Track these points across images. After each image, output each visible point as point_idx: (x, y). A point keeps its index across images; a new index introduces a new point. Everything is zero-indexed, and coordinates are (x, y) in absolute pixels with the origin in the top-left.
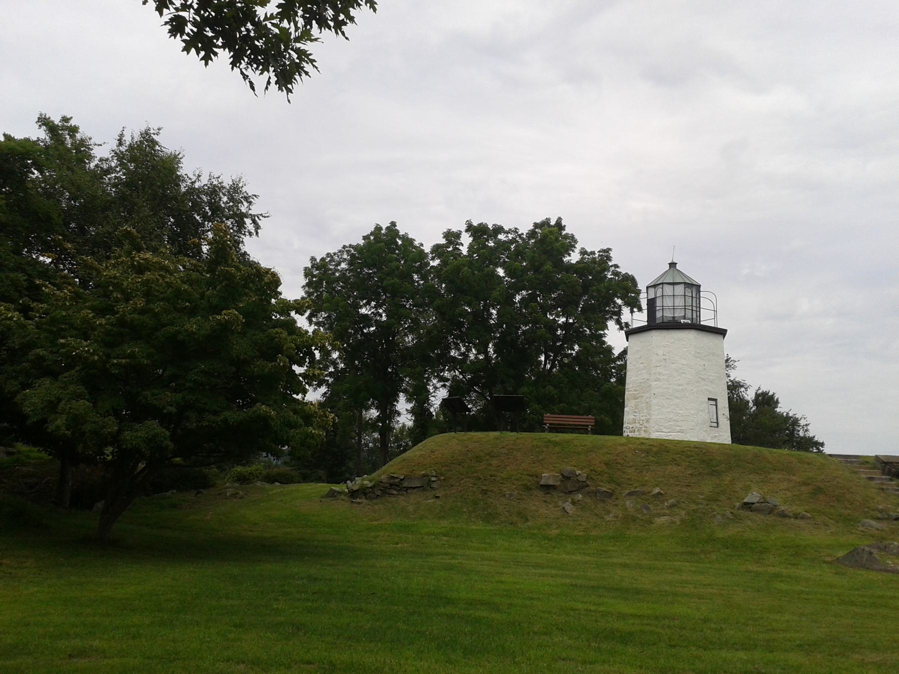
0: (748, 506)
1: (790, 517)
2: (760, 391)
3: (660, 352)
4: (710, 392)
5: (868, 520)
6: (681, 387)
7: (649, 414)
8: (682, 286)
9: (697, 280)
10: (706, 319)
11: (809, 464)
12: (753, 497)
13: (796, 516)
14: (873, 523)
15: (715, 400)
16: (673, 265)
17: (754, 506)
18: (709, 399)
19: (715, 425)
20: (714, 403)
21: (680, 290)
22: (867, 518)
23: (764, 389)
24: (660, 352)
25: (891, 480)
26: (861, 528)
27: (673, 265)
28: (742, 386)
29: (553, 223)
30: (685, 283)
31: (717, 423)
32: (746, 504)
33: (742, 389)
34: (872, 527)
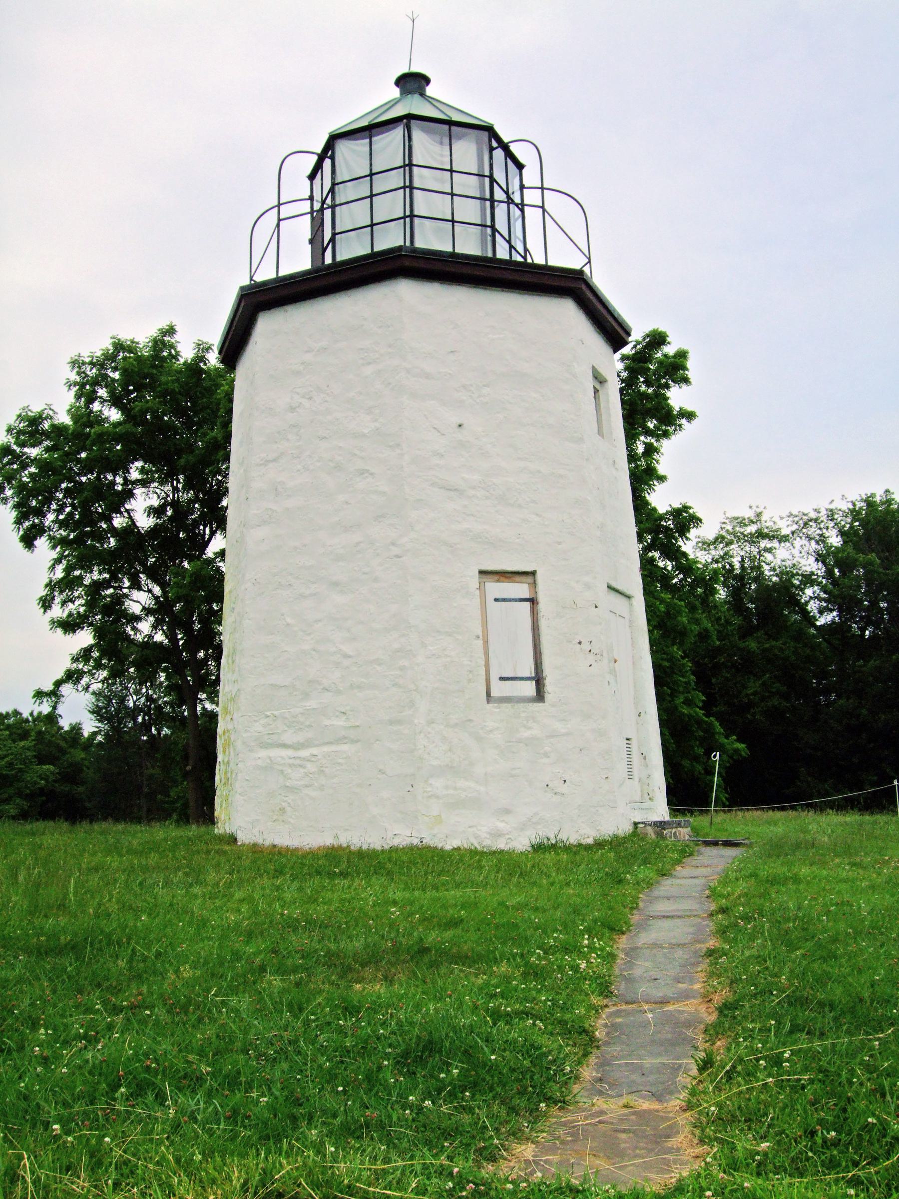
20: (521, 589)
31: (539, 680)
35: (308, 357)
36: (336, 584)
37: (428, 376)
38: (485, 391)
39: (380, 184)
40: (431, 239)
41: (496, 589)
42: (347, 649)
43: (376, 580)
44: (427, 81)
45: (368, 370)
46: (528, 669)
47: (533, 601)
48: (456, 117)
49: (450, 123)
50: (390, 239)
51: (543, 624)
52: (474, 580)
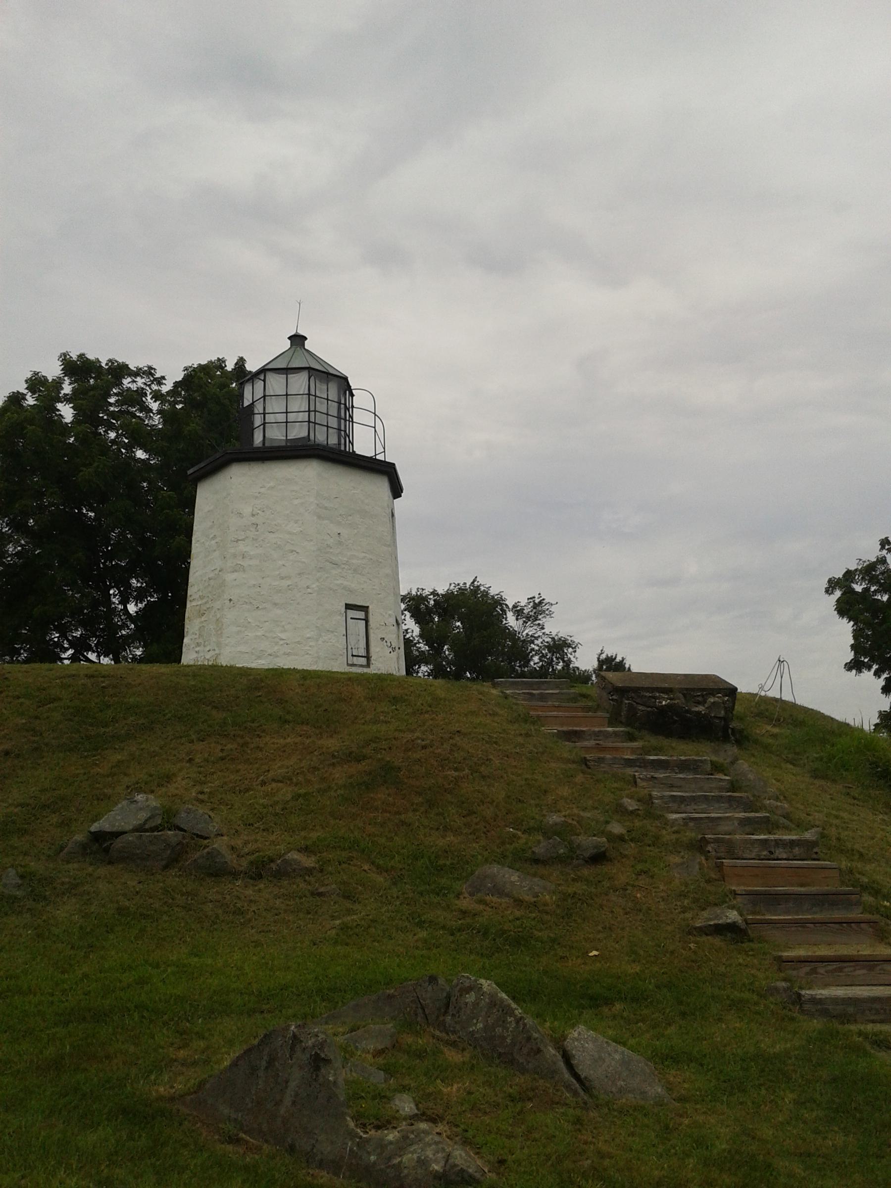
0: (102, 844)
1: (234, 874)
2: (603, 656)
3: (247, 510)
4: (351, 591)
5: (495, 869)
6: (285, 583)
7: (219, 644)
8: (304, 376)
9: (341, 366)
10: (363, 444)
11: (395, 700)
12: (122, 816)
13: (260, 870)
14: (511, 877)
15: (365, 609)
16: (298, 340)
17: (118, 843)
18: (348, 607)
19: (363, 661)
20: (361, 615)
21: (299, 383)
22: (501, 859)
23: (609, 652)
24: (247, 510)
25: (631, 738)
26: (465, 903)
27: (298, 340)
28: (569, 646)
29: (230, 366)
30: (309, 369)
31: (368, 657)
32: (99, 837)
33: (570, 650)
34: (499, 891)
35: (262, 490)
36: (276, 604)
37: (326, 508)
38: (350, 518)
39: (312, 420)
40: (320, 437)
41: (351, 613)
42: (283, 636)
43: (298, 604)
44: (306, 338)
45: (296, 502)
46: (363, 652)
47: (366, 620)
48: (332, 371)
49: (328, 374)
50: (298, 432)
51: (371, 632)
52: (343, 609)
